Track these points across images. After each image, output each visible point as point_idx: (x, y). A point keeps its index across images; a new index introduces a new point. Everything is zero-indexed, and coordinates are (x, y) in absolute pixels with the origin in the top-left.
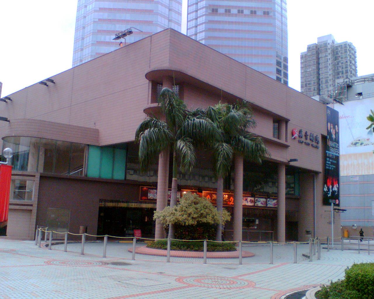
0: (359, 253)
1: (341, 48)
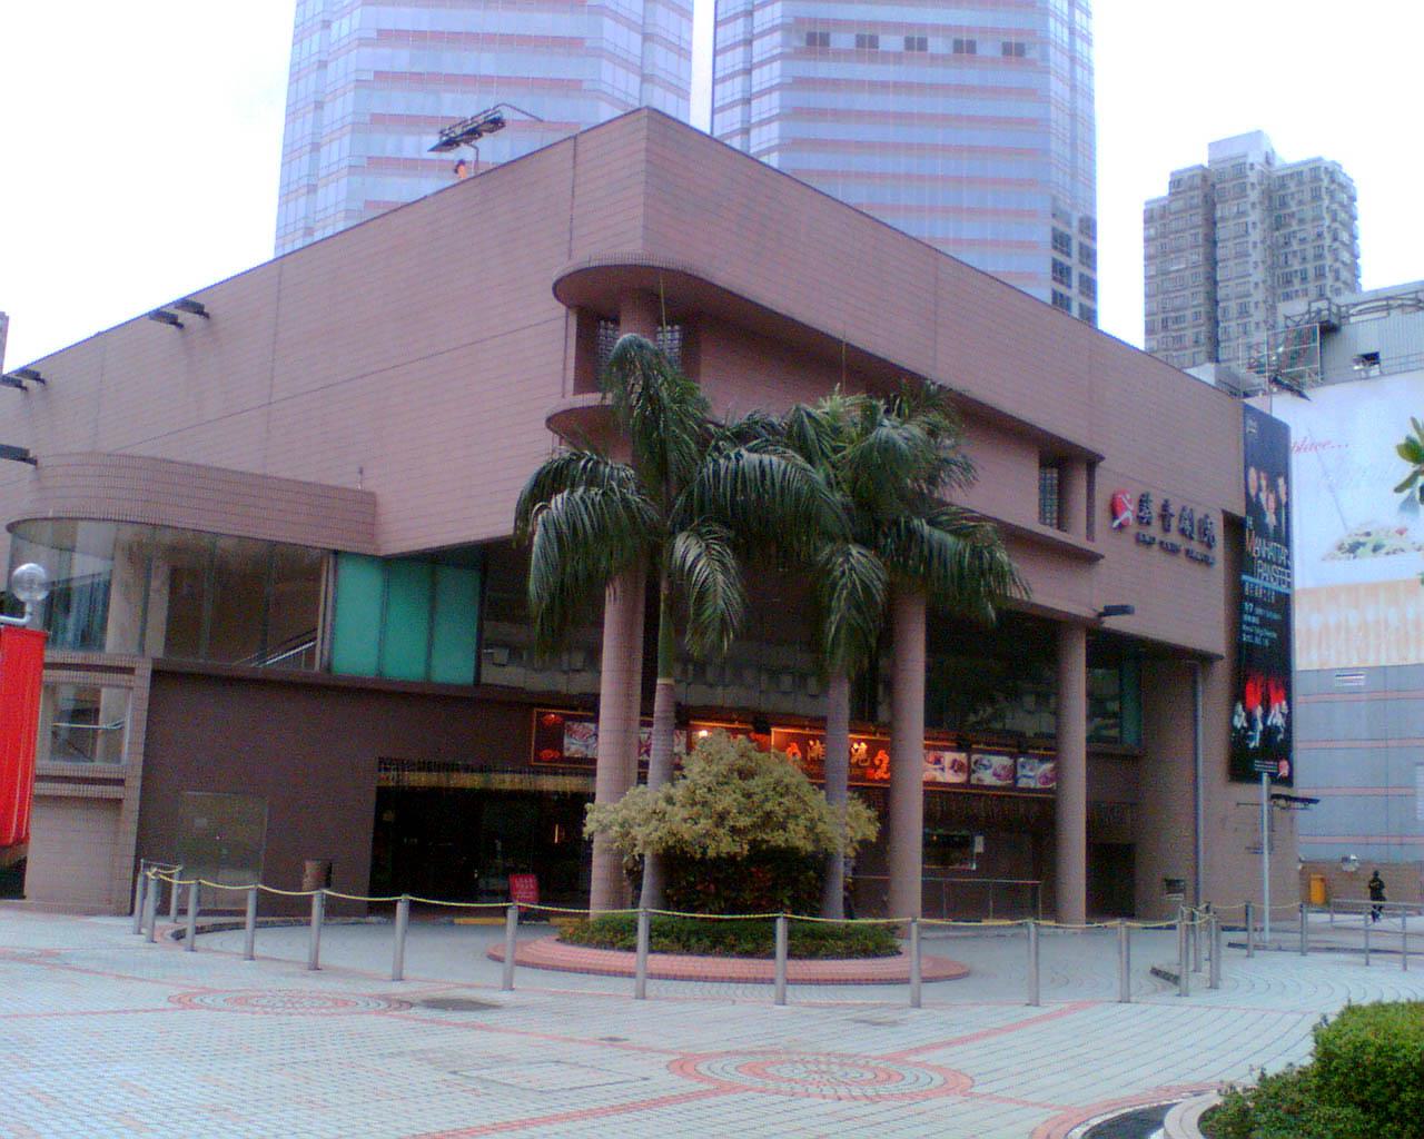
0: (1367, 964)
1: (1300, 183)
